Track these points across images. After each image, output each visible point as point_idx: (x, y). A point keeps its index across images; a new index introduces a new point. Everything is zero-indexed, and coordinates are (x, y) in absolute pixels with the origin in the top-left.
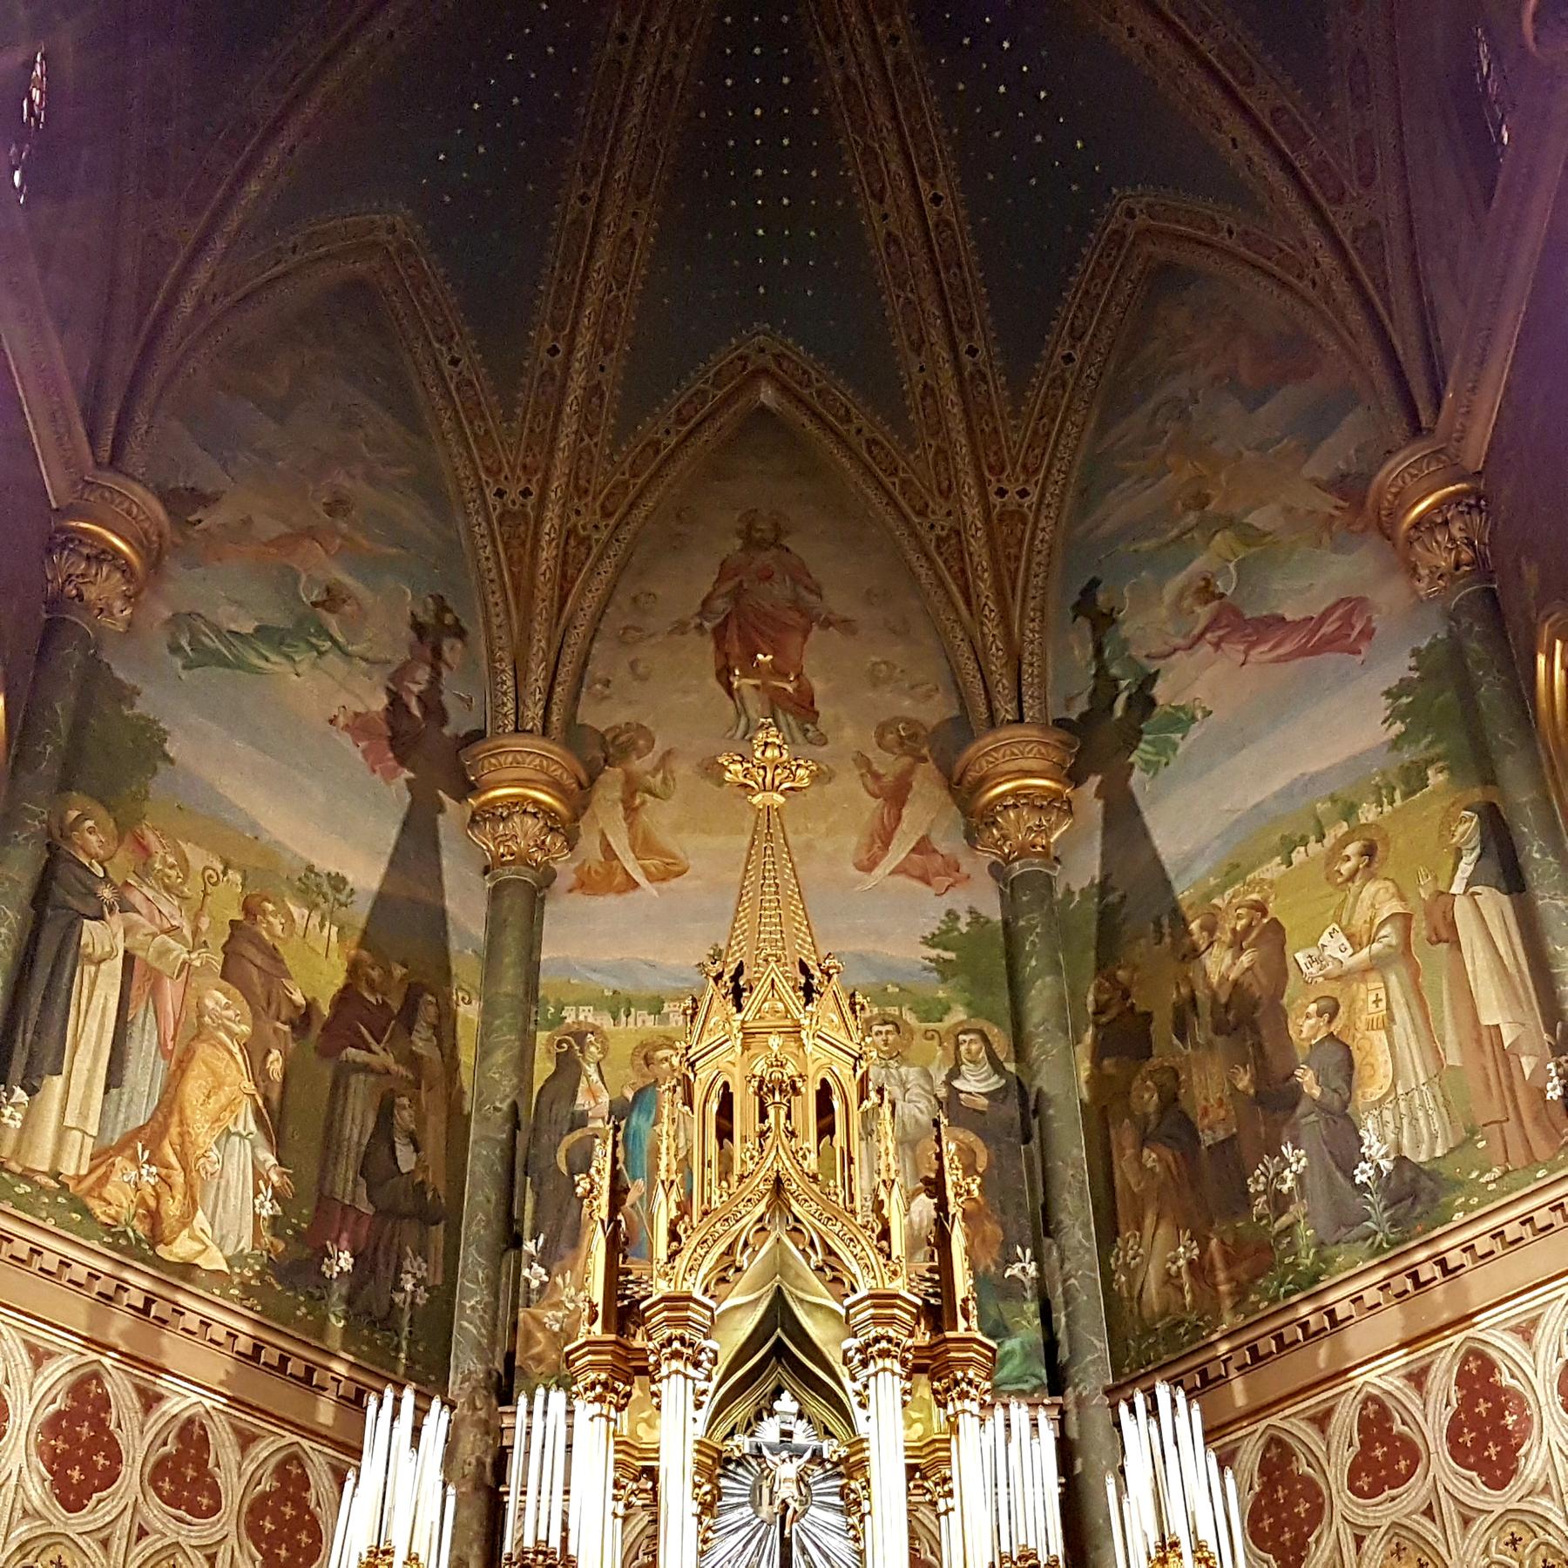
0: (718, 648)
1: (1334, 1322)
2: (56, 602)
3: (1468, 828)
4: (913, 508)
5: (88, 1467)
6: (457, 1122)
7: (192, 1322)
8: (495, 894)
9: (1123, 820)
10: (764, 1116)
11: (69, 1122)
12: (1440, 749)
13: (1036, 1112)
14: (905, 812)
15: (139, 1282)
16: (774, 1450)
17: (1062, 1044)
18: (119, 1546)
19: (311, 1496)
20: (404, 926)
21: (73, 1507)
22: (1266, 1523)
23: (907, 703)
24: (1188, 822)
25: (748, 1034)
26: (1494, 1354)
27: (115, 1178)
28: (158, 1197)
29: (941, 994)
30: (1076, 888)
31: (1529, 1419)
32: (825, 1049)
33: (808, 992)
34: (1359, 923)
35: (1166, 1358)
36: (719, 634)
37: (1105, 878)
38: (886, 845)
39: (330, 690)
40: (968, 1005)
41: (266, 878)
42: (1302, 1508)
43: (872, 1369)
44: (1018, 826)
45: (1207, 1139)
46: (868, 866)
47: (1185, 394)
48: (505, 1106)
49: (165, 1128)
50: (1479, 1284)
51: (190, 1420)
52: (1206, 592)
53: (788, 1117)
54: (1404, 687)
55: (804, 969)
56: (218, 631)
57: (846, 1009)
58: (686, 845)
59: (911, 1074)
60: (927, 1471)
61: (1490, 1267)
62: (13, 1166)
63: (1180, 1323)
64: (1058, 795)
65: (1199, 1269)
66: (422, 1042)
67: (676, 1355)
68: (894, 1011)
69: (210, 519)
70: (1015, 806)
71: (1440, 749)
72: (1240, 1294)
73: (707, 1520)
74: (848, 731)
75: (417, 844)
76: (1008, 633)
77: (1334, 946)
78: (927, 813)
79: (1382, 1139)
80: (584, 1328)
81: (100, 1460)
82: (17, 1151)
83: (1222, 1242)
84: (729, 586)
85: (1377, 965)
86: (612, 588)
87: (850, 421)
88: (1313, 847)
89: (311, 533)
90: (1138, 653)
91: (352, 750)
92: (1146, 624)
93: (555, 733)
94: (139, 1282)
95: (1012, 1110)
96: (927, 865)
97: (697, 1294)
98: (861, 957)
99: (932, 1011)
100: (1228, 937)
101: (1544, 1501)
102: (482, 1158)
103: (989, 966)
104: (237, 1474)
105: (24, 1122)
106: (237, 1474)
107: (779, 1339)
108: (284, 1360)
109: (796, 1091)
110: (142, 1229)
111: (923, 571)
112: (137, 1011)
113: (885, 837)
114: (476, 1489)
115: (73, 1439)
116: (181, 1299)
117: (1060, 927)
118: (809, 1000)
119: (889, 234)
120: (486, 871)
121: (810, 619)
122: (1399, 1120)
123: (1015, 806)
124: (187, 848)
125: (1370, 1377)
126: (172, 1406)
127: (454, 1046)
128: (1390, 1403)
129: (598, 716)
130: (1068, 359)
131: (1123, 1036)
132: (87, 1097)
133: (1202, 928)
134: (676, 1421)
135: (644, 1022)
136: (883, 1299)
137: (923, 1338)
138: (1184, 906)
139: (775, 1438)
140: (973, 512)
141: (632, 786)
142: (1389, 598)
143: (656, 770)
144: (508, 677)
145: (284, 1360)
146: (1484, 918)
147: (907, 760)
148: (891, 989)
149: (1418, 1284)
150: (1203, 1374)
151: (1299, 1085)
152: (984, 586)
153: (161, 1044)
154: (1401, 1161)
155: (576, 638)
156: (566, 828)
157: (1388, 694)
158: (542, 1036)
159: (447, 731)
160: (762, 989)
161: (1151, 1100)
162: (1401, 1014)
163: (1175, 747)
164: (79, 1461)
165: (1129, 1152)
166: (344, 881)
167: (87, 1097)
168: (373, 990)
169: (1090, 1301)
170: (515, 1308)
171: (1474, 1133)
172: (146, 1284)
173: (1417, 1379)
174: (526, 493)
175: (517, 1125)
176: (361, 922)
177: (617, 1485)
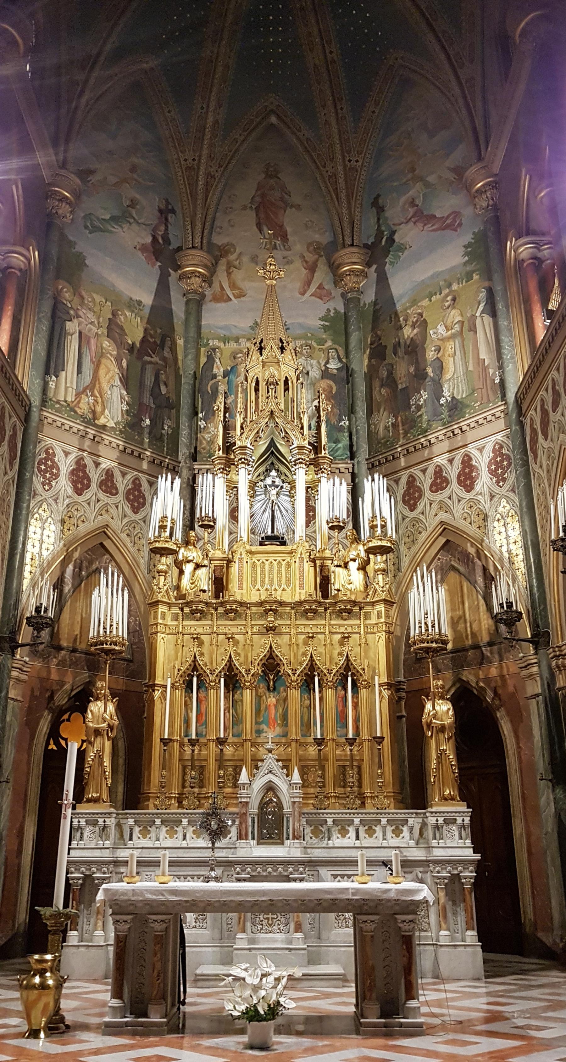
0: (257, 215)
1: (430, 444)
2: (49, 215)
3: (483, 295)
5: (82, 483)
6: (178, 377)
7: (107, 443)
8: (187, 303)
9: (383, 281)
10: (268, 392)
11: (68, 385)
12: (478, 266)
13: (351, 376)
14: (315, 274)
15: (91, 432)
16: (270, 486)
17: (360, 355)
18: (92, 504)
19: (142, 489)
20: (160, 316)
21: (80, 495)
22: (407, 498)
23: (317, 236)
24: (401, 284)
25: (264, 364)
26: (472, 456)
27: (82, 401)
28: (94, 406)
29: (324, 337)
30: (367, 303)
31: (479, 474)
32: (287, 366)
33: (282, 349)
34: (449, 323)
35: (383, 451)
36: (257, 210)
37: (376, 300)
38: (309, 285)
39: (134, 236)
40: (332, 340)
41: (120, 303)
42: (417, 495)
43: (297, 467)
44: (350, 281)
45: (400, 387)
46: (303, 294)
47: (410, 129)
48: (192, 373)
49: (95, 385)
50: (470, 436)
51: (108, 470)
52: (412, 203)
53: (275, 392)
55: (281, 341)
56: (98, 219)
57: (294, 354)
58: (246, 285)
59: (314, 362)
60: (312, 489)
61: (474, 431)
62: (54, 399)
63: (388, 441)
64: (363, 271)
67: (243, 463)
68: (309, 342)
69: (94, 179)
71: (478, 266)
72: (406, 433)
73: (252, 500)
74: (298, 247)
75: (163, 289)
76: (350, 212)
77: (441, 329)
78: (322, 275)
79: (449, 391)
80: (217, 452)
81: (85, 482)
82: (54, 396)
83: (402, 419)
84: (259, 192)
85: (453, 337)
86: (222, 193)
87: (301, 131)
88: (438, 296)
89: (125, 181)
90: (391, 223)
91: (141, 257)
92: (395, 211)
93: (205, 248)
94: (91, 432)
95: (344, 373)
96: (321, 294)
97: (249, 446)
98: (300, 324)
99: (321, 342)
100: (411, 323)
101: (480, 497)
102: (185, 390)
103: (339, 326)
104: (122, 484)
105: (56, 386)
106: (122, 484)
107: (272, 451)
108: (132, 452)
109: (277, 384)
110: (90, 416)
111: (323, 188)
112: (84, 349)
113: (308, 283)
114: (188, 485)
115: (78, 476)
116: (103, 436)
118: (282, 353)
119: (315, 64)
120: (184, 295)
121: (287, 205)
122: (454, 386)
124: (95, 295)
125: (439, 460)
126: (103, 466)
127: (176, 354)
128: (443, 467)
129: (219, 240)
130: (374, 112)
131: (378, 353)
132: (72, 378)
133: (404, 320)
134: (243, 477)
135: (233, 345)
136: (300, 448)
137: (312, 456)
138: (399, 311)
139: (270, 483)
140: (340, 168)
141: (230, 265)
142: (468, 212)
143: (237, 259)
144: (189, 227)
145: (132, 452)
146: (484, 324)
147: (317, 256)
148: (309, 335)
149: (454, 435)
150: (393, 456)
151: (427, 373)
152: (343, 196)
153: (91, 359)
154: (453, 398)
155: (211, 212)
156: (208, 280)
157: (465, 246)
158: (203, 349)
159: (171, 248)
160: (268, 348)
161: (385, 373)
162: (458, 353)
163: (400, 257)
164: (80, 482)
165: (377, 389)
166: (141, 302)
167: (72, 378)
168: (152, 337)
169: (363, 434)
170: (197, 434)
171: (474, 391)
172: (93, 432)
173: (451, 461)
174: (194, 160)
175: (196, 378)
176: (147, 316)
177: (227, 491)
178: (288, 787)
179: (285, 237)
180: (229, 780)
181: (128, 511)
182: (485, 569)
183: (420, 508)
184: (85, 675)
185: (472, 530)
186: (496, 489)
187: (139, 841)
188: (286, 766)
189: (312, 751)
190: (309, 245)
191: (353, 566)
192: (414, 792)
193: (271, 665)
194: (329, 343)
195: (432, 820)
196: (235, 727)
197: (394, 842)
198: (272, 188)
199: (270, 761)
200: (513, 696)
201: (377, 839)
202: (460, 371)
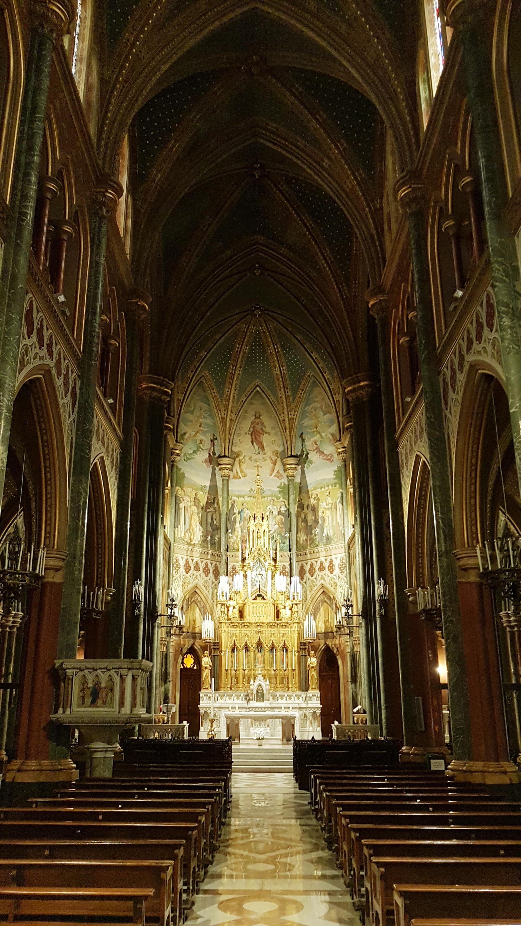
2: (172, 462)
8: (223, 480)
9: (303, 473)
20: (213, 488)
41: (196, 488)
54: (335, 471)
58: (247, 471)
59: (275, 507)
65: (306, 540)
66: (216, 506)
72: (310, 544)
74: (269, 452)
75: (214, 474)
77: (325, 504)
78: (279, 466)
85: (328, 509)
92: (309, 444)
94: (190, 548)
95: (287, 513)
103: (286, 490)
104: (202, 566)
117: (295, 487)
122: (328, 530)
131: (301, 506)
141: (240, 461)
152: (288, 431)
173: (326, 560)
178: (265, 686)
179: (263, 448)
181: (204, 576)
182: (336, 604)
183: (314, 576)
184: (192, 641)
185: (332, 589)
186: (340, 575)
187: (220, 701)
188: (264, 677)
189: (273, 672)
190: (273, 452)
191: (287, 608)
192: (305, 687)
193: (259, 644)
194: (281, 499)
195: (308, 695)
197: (297, 701)
198: (258, 424)
199: (260, 677)
200: (343, 651)
201: (292, 701)
202: (331, 525)
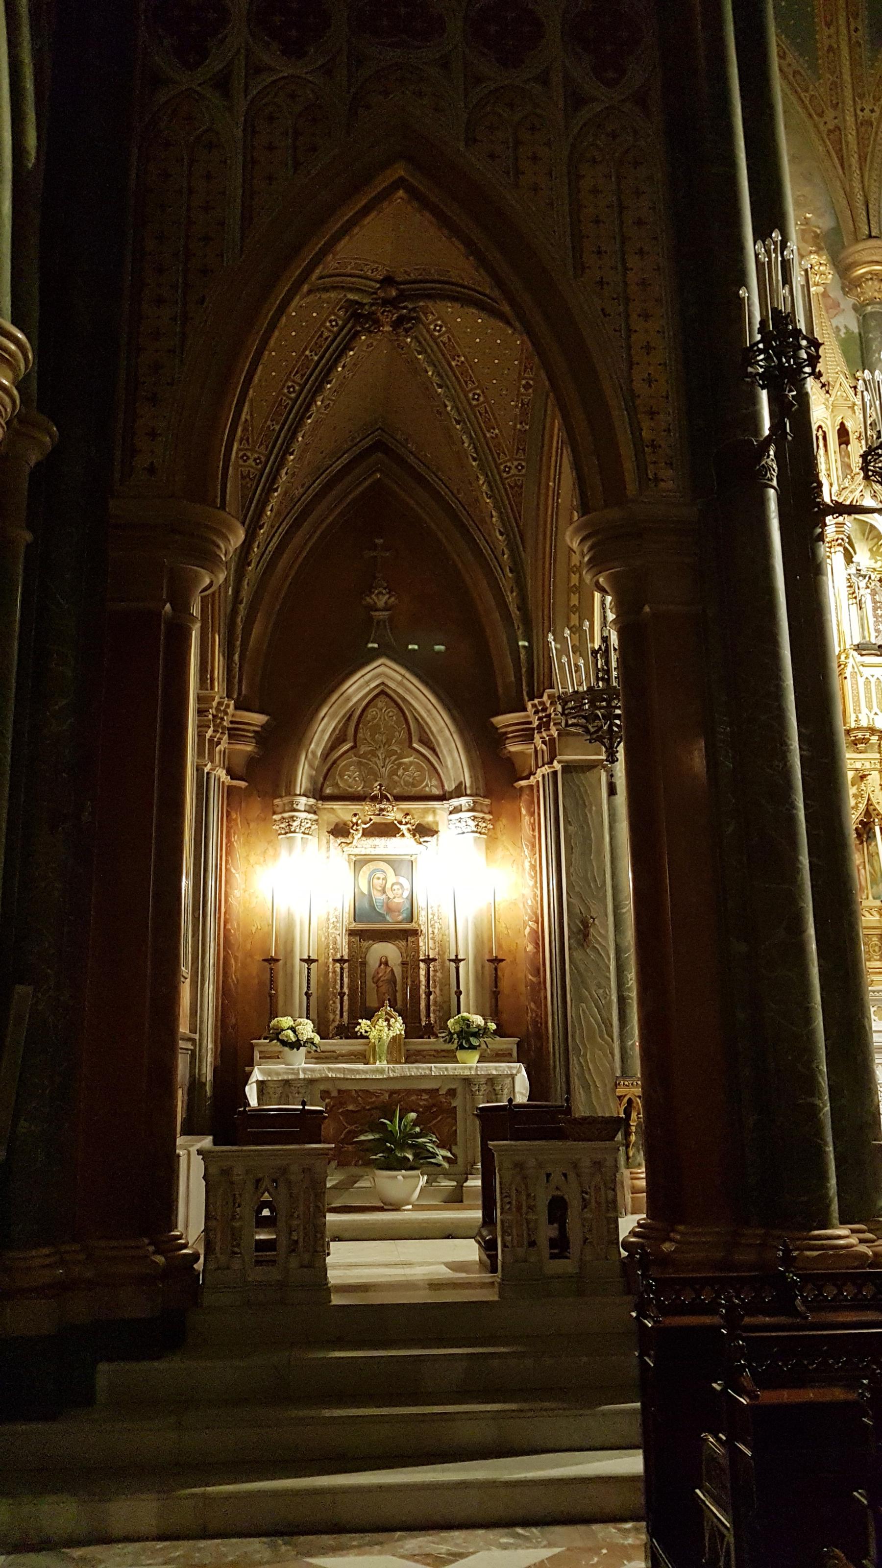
4: (815, 112)
70: (871, 279)
123: (871, 279)
180: (874, 951)
196: (875, 887)
